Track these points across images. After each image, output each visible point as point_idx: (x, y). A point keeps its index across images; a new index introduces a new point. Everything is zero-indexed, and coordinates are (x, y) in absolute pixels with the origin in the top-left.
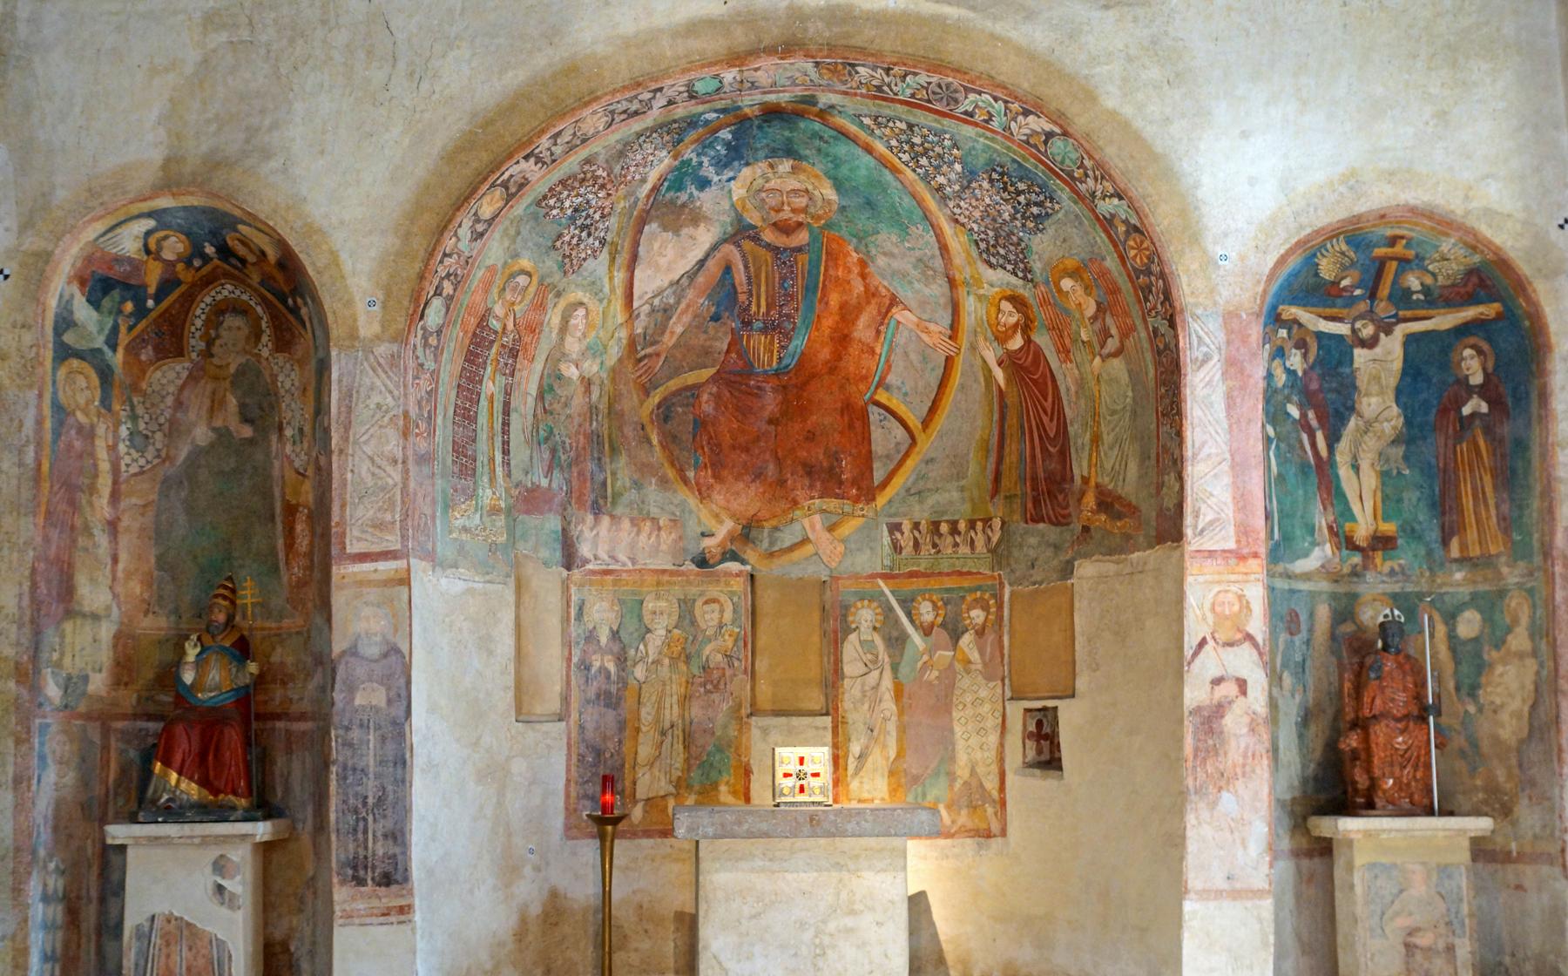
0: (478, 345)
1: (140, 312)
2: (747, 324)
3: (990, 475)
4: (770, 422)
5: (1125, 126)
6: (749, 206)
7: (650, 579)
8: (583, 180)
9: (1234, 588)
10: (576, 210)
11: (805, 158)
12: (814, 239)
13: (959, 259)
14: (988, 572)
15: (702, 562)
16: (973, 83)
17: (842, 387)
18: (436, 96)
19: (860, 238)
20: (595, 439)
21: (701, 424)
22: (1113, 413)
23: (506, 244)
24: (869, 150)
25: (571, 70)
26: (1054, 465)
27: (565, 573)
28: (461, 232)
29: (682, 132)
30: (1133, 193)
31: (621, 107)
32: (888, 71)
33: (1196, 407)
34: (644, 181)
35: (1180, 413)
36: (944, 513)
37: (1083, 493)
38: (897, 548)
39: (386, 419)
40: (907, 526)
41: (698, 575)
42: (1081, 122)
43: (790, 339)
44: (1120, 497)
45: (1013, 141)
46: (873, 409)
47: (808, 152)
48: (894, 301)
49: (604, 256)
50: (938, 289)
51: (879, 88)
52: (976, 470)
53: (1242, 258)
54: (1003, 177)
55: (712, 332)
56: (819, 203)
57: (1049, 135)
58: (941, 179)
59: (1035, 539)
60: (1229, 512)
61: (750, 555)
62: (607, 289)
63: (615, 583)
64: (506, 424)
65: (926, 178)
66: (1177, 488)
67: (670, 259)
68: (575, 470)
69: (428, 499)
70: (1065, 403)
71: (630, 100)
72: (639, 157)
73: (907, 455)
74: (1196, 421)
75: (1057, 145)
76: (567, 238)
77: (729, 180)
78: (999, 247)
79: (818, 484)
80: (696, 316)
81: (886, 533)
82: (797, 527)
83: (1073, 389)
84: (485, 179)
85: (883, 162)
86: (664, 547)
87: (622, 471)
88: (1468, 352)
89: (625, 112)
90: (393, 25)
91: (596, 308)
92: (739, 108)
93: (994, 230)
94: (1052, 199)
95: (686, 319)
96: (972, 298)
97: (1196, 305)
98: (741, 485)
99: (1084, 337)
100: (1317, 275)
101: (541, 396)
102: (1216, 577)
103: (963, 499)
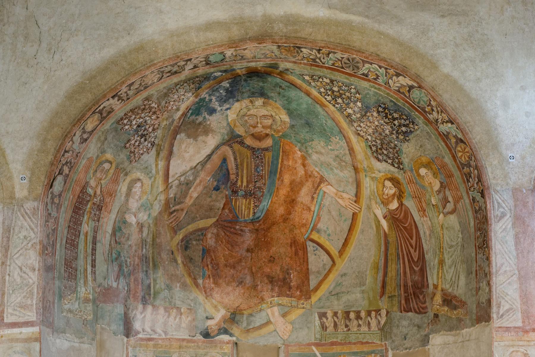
0: (80, 203)
2: (235, 192)
3: (380, 285)
4: (248, 250)
5: (455, 82)
6: (238, 124)
7: (175, 344)
8: (144, 109)
9: (522, 350)
10: (139, 126)
11: (272, 98)
12: (275, 143)
14: (379, 342)
15: (206, 335)
16: (367, 58)
17: (291, 231)
18: (64, 62)
19: (303, 143)
20: (145, 259)
21: (206, 252)
22: (451, 247)
23: (99, 145)
24: (308, 94)
25: (140, 48)
26: (416, 278)
27: (125, 339)
28: (74, 138)
29: (201, 83)
30: (460, 121)
31: (167, 69)
32: (319, 51)
33: (497, 243)
34: (178, 109)
35: (488, 247)
36: (353, 306)
37: (434, 294)
38: (324, 327)
39: (30, 245)
40: (330, 314)
41: (204, 342)
42: (429, 79)
43: (260, 202)
44: (455, 297)
45: (390, 90)
46: (309, 243)
47: (273, 94)
48: (322, 180)
49: (153, 152)
50: (348, 174)
51: (314, 60)
52: (371, 281)
53: (523, 158)
54: (386, 111)
55: (214, 196)
56: (279, 123)
57: (411, 88)
58: (350, 111)
59: (406, 322)
60: (518, 304)
61: (235, 330)
62: (154, 171)
63: (155, 346)
64: (94, 249)
65: (341, 110)
66: (487, 290)
67: (191, 154)
68: (132, 278)
69: (51, 292)
70: (423, 241)
71: (173, 66)
72: (176, 96)
73: (330, 271)
74: (498, 251)
75: (416, 94)
76: (133, 142)
77: (227, 109)
78: (383, 150)
79: (277, 289)
80: (205, 187)
81: (317, 318)
82: (263, 314)
83: (428, 233)
84: (90, 109)
85: (316, 101)
86: (183, 325)
87: (160, 279)
89: (169, 72)
90: (39, 22)
91: (147, 182)
92: (234, 70)
93: (380, 140)
94: (413, 123)
95: (200, 189)
96: (368, 179)
97: (497, 184)
98: (230, 288)
99: (434, 202)
101: (114, 234)
102: (511, 343)
103: (363, 298)
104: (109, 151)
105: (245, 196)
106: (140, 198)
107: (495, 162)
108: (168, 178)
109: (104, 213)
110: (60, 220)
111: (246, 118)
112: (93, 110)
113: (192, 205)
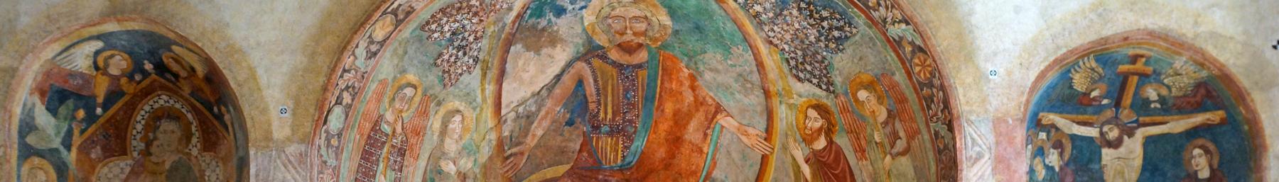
0: (372, 145)
1: (91, 118)
2: (596, 128)
6: (598, 30)
8: (460, 8)
10: (454, 34)
12: (652, 57)
13: (772, 74)
23: (396, 62)
28: (358, 52)
30: (918, 19)
43: (632, 141)
48: (719, 109)
49: (477, 71)
50: (756, 99)
53: (1009, 73)
55: (567, 135)
56: (657, 28)
58: (758, 8)
62: (479, 99)
76: (446, 57)
77: (582, 8)
80: (554, 122)
84: (378, 8)
88: (1197, 151)
91: (470, 115)
93: (803, 50)
94: (850, 25)
95: (546, 124)
96: (783, 107)
97: (971, 112)
100: (1071, 87)
104: (412, 70)
105: (610, 134)
106: (461, 137)
107: (969, 80)
108: (500, 109)
109: (408, 160)
110: (342, 170)
111: (610, 21)
112: (383, 9)
113: (536, 146)
